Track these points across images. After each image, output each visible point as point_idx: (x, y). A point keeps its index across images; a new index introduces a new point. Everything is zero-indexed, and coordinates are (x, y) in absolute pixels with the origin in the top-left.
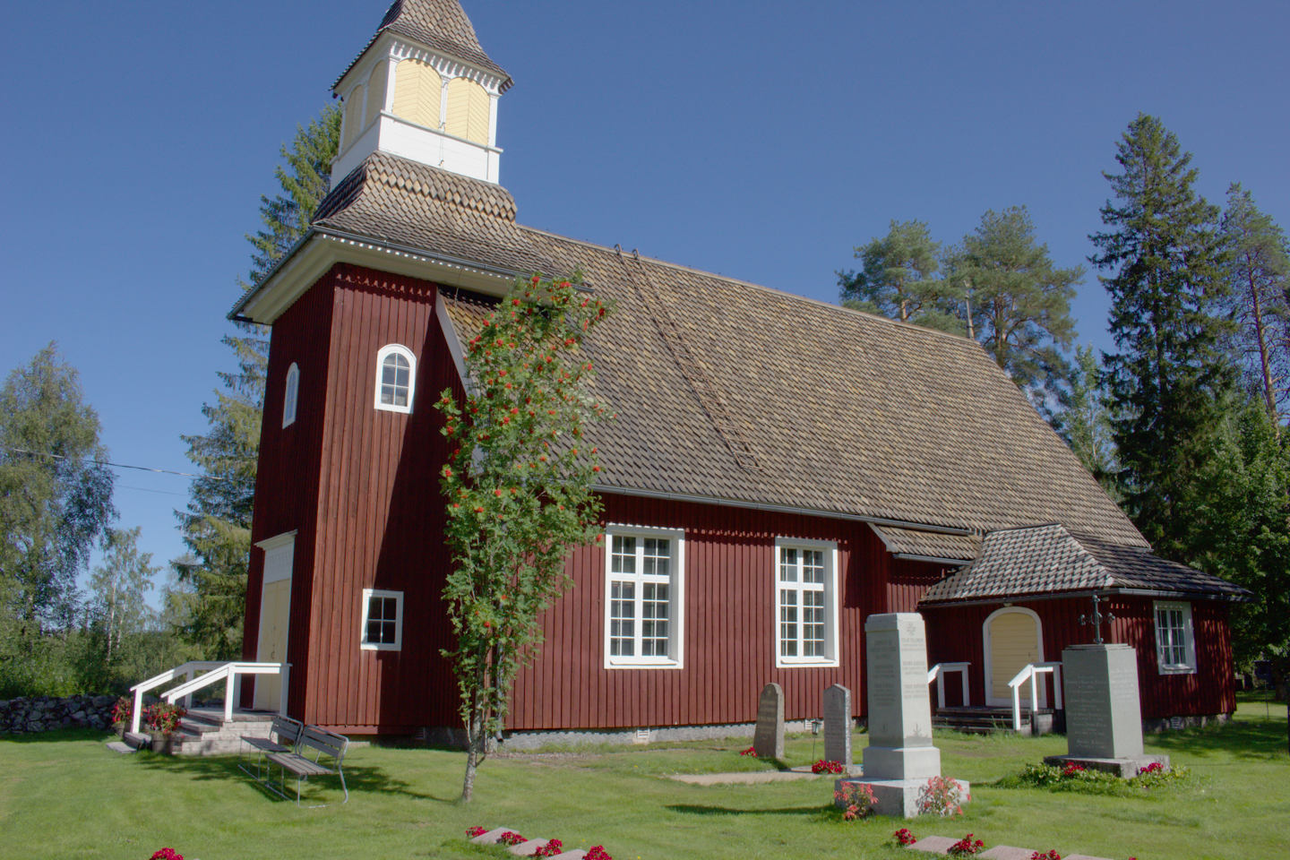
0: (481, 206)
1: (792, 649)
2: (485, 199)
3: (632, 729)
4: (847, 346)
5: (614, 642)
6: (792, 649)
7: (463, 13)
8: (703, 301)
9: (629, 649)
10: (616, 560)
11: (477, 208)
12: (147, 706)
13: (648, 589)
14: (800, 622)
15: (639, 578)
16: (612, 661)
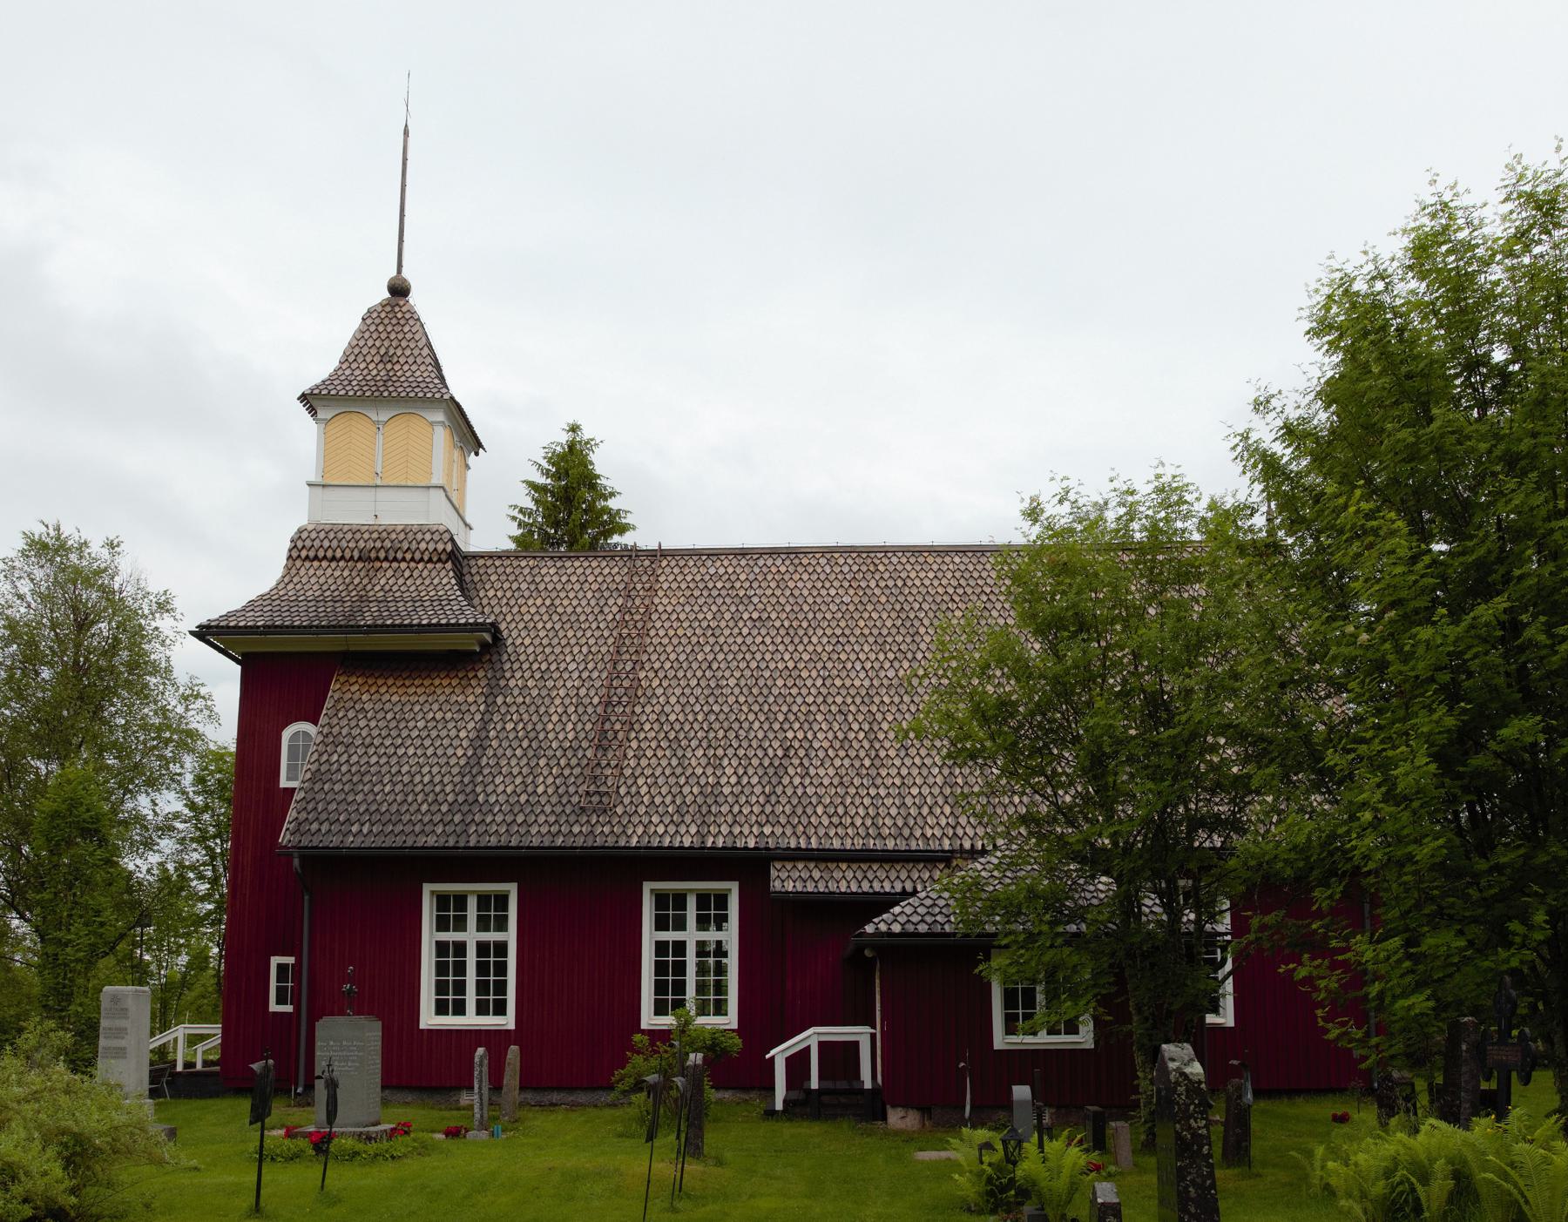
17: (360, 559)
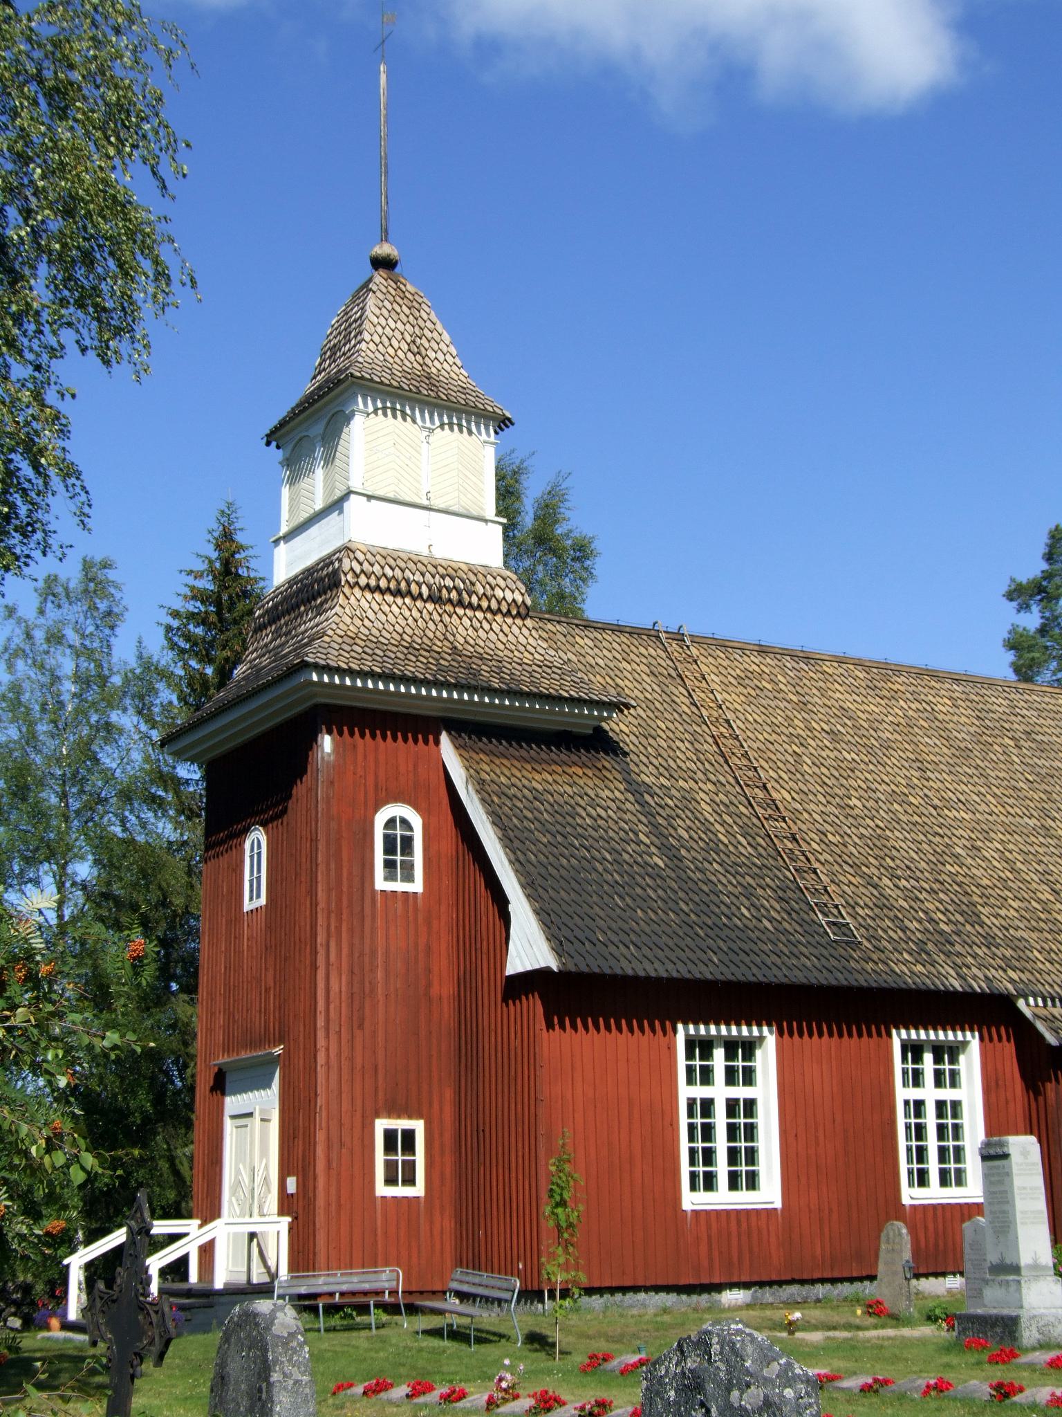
0: (485, 604)
1: (922, 1179)
2: (489, 592)
3: (719, 1288)
4: (990, 740)
5: (693, 1176)
6: (922, 1179)
7: (439, 327)
8: (780, 696)
9: (710, 1182)
10: (690, 1070)
11: (479, 607)
12: (991, 1183)
13: (940, 1105)
14: (721, 1144)
15: (720, 1092)
16: (692, 1200)
17: (430, 597)
